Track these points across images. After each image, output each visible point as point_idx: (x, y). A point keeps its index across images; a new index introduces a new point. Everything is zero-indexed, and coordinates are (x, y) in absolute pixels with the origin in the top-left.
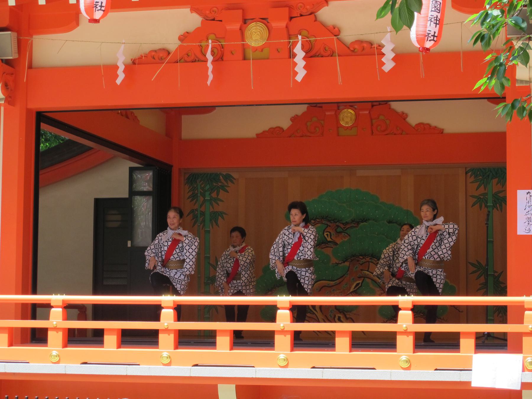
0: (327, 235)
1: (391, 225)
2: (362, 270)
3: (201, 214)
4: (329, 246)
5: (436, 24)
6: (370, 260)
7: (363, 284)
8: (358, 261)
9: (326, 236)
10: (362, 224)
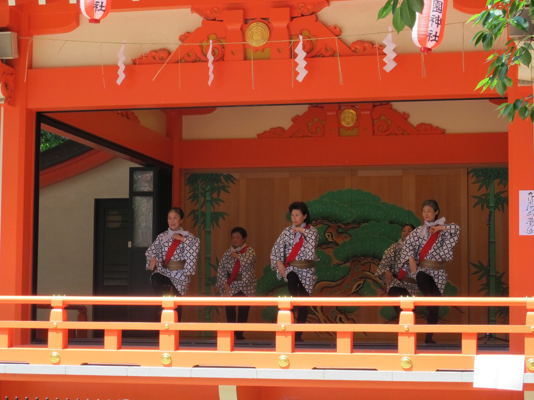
0: (329, 235)
1: (392, 225)
2: (363, 271)
3: (201, 214)
4: (330, 246)
5: (438, 24)
6: (371, 261)
7: (364, 285)
8: (359, 262)
9: (327, 237)
10: (363, 224)
